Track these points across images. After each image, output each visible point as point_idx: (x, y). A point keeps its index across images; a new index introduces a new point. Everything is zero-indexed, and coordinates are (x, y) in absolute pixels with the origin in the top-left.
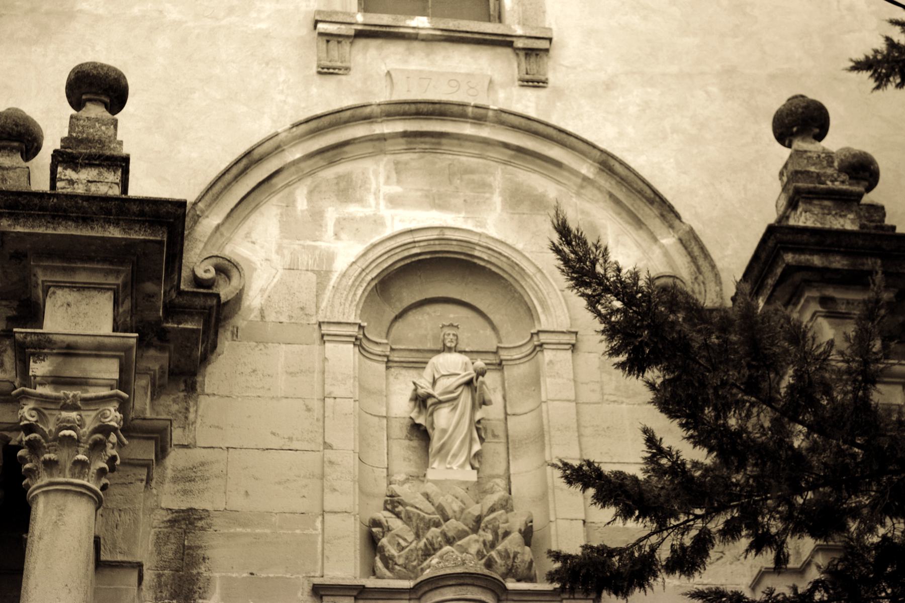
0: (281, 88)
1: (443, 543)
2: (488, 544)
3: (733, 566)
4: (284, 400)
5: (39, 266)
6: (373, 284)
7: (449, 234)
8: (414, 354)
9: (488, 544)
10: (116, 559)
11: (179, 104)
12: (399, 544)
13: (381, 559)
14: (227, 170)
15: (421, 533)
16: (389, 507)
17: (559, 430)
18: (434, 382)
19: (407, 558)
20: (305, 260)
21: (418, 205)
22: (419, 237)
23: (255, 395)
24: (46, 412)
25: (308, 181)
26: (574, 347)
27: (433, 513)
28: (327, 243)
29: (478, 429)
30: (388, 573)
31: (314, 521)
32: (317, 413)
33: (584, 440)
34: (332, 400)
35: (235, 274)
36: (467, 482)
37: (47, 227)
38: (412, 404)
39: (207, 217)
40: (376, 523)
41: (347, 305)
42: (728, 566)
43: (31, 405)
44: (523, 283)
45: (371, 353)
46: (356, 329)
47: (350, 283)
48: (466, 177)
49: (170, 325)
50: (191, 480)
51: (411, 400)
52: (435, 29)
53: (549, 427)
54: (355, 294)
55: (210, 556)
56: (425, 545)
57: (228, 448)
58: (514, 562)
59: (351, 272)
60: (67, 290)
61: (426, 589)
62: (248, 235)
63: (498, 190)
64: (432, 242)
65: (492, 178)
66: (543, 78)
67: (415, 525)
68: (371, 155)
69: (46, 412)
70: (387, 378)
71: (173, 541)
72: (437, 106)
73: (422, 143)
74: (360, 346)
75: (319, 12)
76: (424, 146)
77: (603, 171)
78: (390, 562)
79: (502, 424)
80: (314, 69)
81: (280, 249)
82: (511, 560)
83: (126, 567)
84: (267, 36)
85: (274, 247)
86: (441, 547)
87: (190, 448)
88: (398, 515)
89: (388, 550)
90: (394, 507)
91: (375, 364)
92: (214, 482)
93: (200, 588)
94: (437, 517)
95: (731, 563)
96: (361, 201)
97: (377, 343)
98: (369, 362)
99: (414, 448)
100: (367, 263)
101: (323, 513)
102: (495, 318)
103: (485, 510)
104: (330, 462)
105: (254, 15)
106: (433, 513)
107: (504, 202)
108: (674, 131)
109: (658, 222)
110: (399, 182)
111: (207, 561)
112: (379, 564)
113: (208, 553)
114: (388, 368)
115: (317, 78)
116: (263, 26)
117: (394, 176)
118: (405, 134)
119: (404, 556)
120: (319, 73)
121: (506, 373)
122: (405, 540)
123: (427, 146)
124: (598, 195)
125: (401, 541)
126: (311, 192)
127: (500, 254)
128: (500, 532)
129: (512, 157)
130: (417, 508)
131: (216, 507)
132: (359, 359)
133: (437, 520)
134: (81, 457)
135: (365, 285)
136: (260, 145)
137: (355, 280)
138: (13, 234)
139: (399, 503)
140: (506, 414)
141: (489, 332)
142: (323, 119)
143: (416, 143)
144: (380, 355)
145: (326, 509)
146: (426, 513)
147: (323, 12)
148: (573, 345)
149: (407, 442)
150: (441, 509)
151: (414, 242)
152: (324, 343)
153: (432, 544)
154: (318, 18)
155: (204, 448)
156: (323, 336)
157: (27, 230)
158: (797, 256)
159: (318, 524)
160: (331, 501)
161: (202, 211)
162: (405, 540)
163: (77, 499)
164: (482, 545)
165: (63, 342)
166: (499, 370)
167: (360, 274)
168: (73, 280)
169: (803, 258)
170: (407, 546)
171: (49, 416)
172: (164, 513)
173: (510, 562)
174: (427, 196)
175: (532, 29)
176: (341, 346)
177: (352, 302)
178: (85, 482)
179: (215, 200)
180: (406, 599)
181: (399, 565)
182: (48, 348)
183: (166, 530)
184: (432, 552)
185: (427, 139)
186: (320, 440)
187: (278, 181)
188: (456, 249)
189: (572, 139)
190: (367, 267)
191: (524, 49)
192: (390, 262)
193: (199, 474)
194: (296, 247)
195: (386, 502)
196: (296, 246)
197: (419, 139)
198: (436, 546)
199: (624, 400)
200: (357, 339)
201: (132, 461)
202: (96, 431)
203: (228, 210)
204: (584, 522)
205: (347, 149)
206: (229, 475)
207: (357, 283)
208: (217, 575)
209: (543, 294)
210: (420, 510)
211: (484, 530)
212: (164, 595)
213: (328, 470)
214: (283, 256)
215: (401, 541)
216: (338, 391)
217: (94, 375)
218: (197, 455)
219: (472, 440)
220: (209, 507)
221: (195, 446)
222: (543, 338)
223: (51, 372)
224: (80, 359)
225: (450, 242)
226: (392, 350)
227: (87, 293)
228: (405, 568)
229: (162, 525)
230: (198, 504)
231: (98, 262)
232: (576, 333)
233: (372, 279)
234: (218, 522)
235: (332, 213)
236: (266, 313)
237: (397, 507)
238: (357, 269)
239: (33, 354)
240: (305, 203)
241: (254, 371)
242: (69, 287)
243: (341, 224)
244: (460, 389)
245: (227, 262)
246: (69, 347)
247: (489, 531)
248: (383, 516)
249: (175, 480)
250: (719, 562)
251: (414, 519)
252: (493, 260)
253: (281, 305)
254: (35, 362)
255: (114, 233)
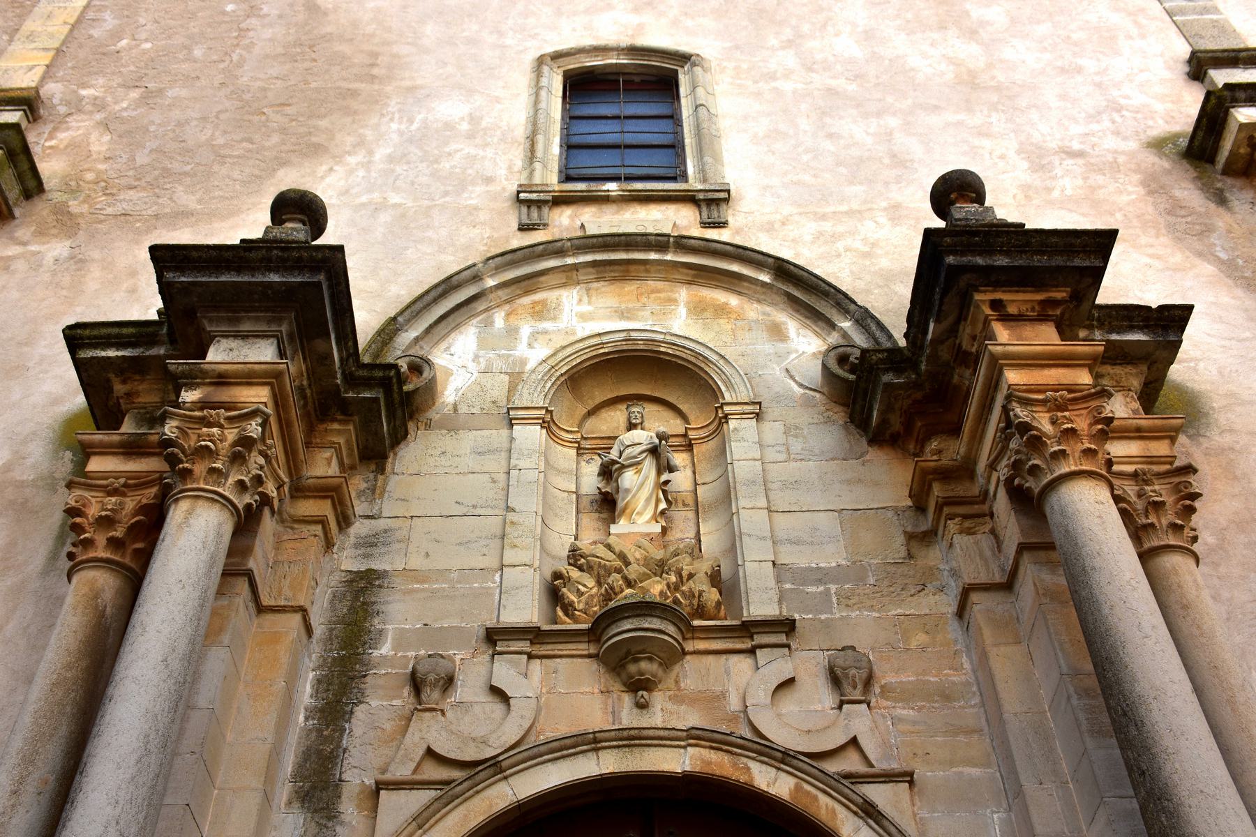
0: (485, 242)
1: (624, 587)
2: (672, 587)
3: (937, 597)
4: (471, 475)
5: (205, 317)
6: (562, 379)
7: (634, 335)
8: (605, 441)
9: (672, 587)
10: (279, 604)
11: (393, 259)
12: (578, 589)
13: (561, 608)
14: (427, 292)
15: (602, 581)
16: (571, 561)
17: (745, 484)
18: (621, 453)
19: (587, 604)
20: (498, 365)
21: (609, 318)
22: (606, 339)
23: (443, 472)
24: (189, 431)
25: (507, 307)
26: (758, 416)
27: (614, 560)
28: (522, 350)
29: (665, 492)
30: (568, 620)
31: (494, 576)
32: (502, 484)
33: (771, 494)
34: (517, 471)
35: (426, 369)
36: (650, 534)
37: (210, 276)
38: (601, 478)
39: (407, 331)
40: (557, 575)
41: (536, 395)
42: (931, 597)
43: (174, 423)
44: (707, 369)
45: (556, 437)
46: (543, 412)
47: (540, 377)
48: (653, 295)
49: (350, 395)
50: (373, 545)
51: (599, 475)
52: (623, 191)
53: (735, 483)
54: (544, 387)
55: (385, 610)
56: (606, 589)
57: (412, 517)
58: (699, 601)
59: (540, 369)
60: (232, 338)
61: (604, 625)
62: (448, 349)
63: (682, 303)
64: (619, 343)
65: (677, 295)
66: (723, 220)
67: (596, 573)
68: (564, 285)
69: (189, 431)
70: (578, 463)
71: (349, 598)
72: (623, 238)
73: (611, 271)
74: (549, 429)
75: (520, 186)
76: (613, 274)
77: (779, 276)
78: (570, 608)
79: (693, 494)
80: (517, 227)
81: (476, 358)
82: (696, 599)
83: (288, 611)
84: (476, 208)
85: (471, 356)
86: (622, 591)
87: (375, 518)
88: (581, 569)
89: (568, 597)
90: (576, 560)
91: (566, 450)
92: (395, 546)
93: (371, 639)
94: (618, 563)
95: (934, 595)
96: (554, 319)
97: (568, 431)
98: (560, 448)
99: (605, 519)
100: (556, 362)
101: (501, 568)
102: (684, 407)
103: (669, 554)
104: (512, 523)
105: (465, 195)
106: (614, 560)
107: (689, 311)
108: (847, 250)
109: (834, 311)
110: (589, 303)
111: (381, 615)
112: (560, 613)
113: (383, 608)
114: (579, 454)
115: (519, 233)
116: (473, 202)
117: (585, 299)
118: (594, 264)
119: (584, 601)
120: (520, 229)
121: (695, 450)
122: (585, 586)
123: (617, 275)
124: (778, 299)
125: (580, 587)
126: (508, 315)
127: (684, 347)
128: (685, 574)
129: (695, 276)
130: (598, 557)
131: (395, 567)
132: (546, 440)
133: (618, 567)
134: (218, 465)
135: (554, 379)
136: (458, 273)
137: (544, 375)
138: (178, 285)
139: (582, 556)
140: (696, 484)
141: (679, 421)
142: (518, 253)
143: (606, 272)
144: (571, 442)
145: (504, 563)
146: (607, 561)
147: (524, 185)
148: (757, 414)
149: (597, 515)
150: (622, 557)
151: (603, 344)
152: (512, 425)
153: (612, 588)
154: (520, 189)
155: (389, 517)
156: (511, 420)
157: (190, 280)
158: (958, 258)
159: (497, 578)
160: (509, 557)
161: (402, 326)
162: (585, 586)
163: (207, 504)
164: (665, 587)
165: (214, 370)
166: (689, 450)
167: (550, 370)
168: (237, 329)
169: (965, 260)
170: (588, 592)
171: (191, 435)
172: (343, 574)
173: (695, 602)
174: (616, 311)
175: (711, 184)
176: (528, 427)
177: (541, 392)
178: (220, 490)
179: (415, 317)
180: (585, 642)
181: (579, 611)
182: (201, 378)
183: (343, 589)
184: (613, 596)
185: (616, 267)
186: (503, 505)
187: (480, 306)
188: (642, 347)
189: (748, 252)
190: (557, 365)
191: (705, 200)
192: (578, 360)
193: (381, 540)
194: (491, 355)
195: (568, 557)
196: (492, 355)
197: (608, 268)
198: (617, 590)
199: (811, 457)
200: (544, 422)
201: (306, 518)
202: (236, 443)
203: (426, 325)
204: (773, 562)
205: (543, 279)
206: (411, 540)
207: (546, 378)
208: (389, 627)
209: (726, 376)
210: (601, 558)
211: (667, 573)
212: (334, 647)
213: (508, 529)
214: (479, 363)
215: (580, 587)
216: (522, 464)
217: (243, 399)
218: (381, 524)
219: (658, 501)
220: (388, 567)
221: (380, 517)
222: (726, 409)
223: (200, 398)
224: (232, 388)
225: (636, 342)
226: (582, 437)
227: (251, 340)
228: (585, 613)
229: (340, 585)
230: (377, 565)
231: (261, 311)
232: (760, 403)
233: (562, 375)
234: (397, 581)
235: (526, 330)
236: (459, 407)
237: (579, 560)
238: (546, 367)
239: (186, 385)
240: (502, 322)
241: (443, 453)
242: (232, 336)
243: (535, 335)
244: (644, 455)
245: (419, 360)
246: (220, 375)
247: (673, 573)
248: (564, 567)
249: (356, 546)
250: (921, 593)
251: (596, 567)
252: (678, 353)
253: (474, 400)
254: (186, 391)
255: (275, 278)
